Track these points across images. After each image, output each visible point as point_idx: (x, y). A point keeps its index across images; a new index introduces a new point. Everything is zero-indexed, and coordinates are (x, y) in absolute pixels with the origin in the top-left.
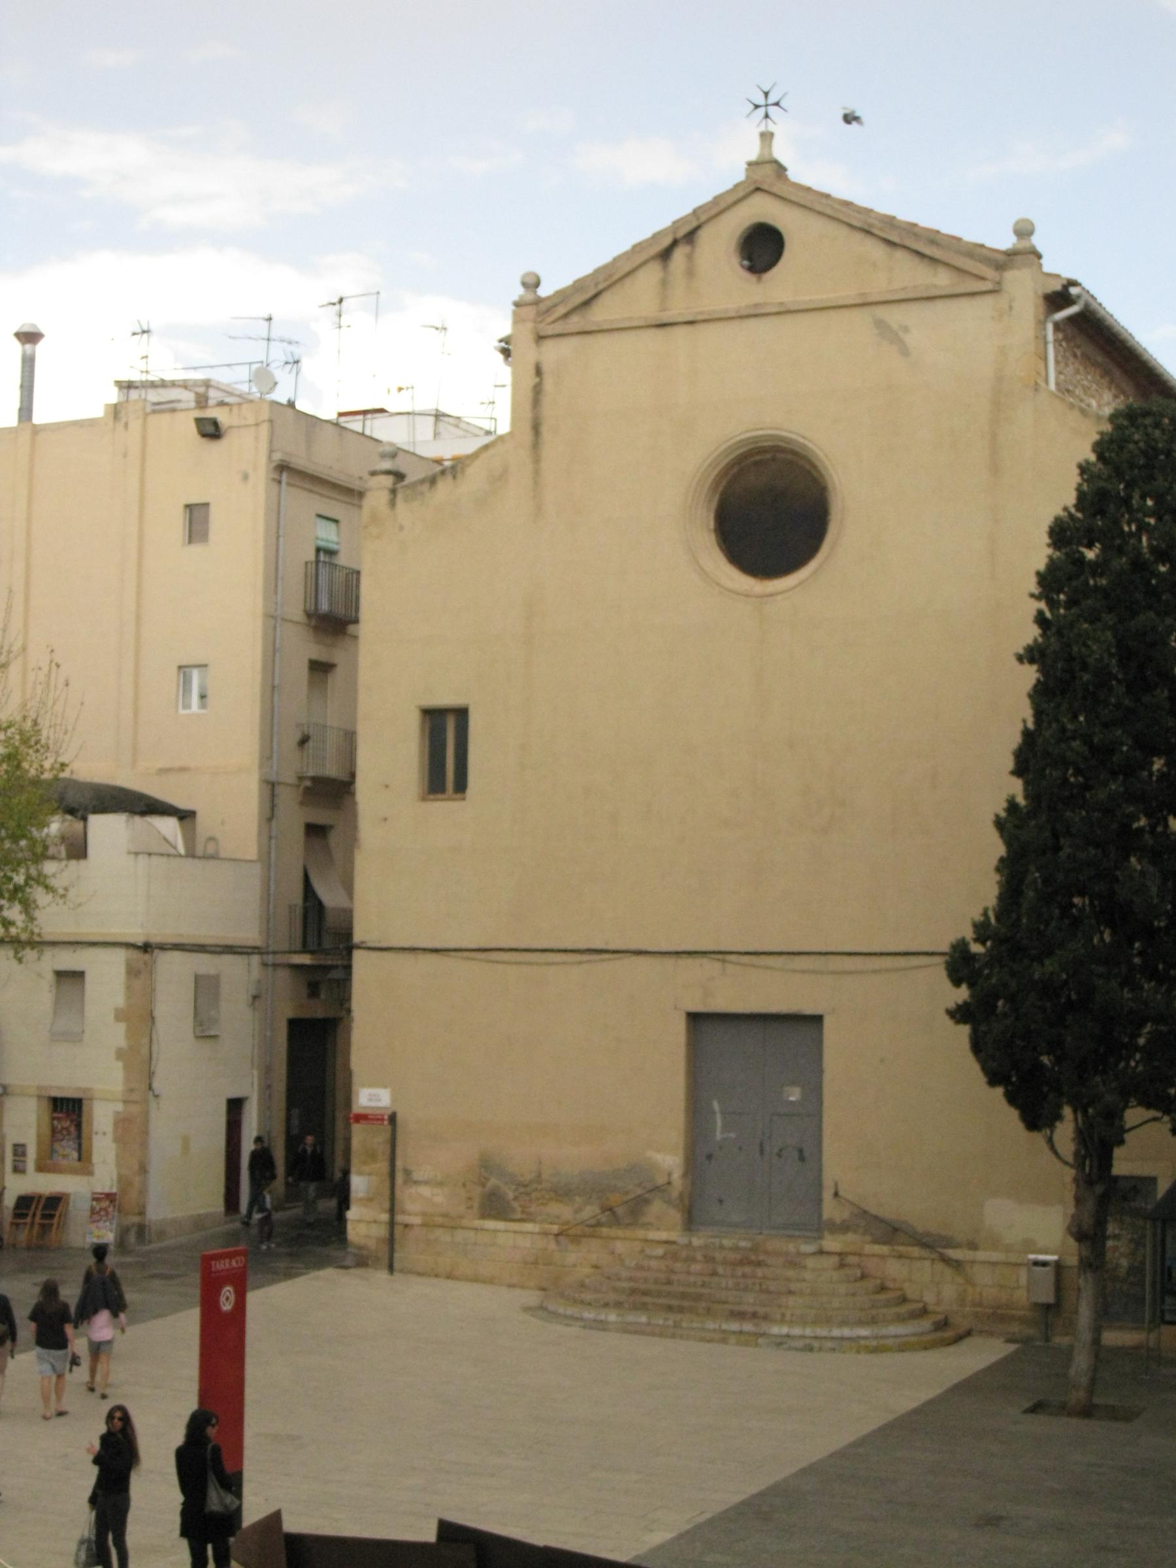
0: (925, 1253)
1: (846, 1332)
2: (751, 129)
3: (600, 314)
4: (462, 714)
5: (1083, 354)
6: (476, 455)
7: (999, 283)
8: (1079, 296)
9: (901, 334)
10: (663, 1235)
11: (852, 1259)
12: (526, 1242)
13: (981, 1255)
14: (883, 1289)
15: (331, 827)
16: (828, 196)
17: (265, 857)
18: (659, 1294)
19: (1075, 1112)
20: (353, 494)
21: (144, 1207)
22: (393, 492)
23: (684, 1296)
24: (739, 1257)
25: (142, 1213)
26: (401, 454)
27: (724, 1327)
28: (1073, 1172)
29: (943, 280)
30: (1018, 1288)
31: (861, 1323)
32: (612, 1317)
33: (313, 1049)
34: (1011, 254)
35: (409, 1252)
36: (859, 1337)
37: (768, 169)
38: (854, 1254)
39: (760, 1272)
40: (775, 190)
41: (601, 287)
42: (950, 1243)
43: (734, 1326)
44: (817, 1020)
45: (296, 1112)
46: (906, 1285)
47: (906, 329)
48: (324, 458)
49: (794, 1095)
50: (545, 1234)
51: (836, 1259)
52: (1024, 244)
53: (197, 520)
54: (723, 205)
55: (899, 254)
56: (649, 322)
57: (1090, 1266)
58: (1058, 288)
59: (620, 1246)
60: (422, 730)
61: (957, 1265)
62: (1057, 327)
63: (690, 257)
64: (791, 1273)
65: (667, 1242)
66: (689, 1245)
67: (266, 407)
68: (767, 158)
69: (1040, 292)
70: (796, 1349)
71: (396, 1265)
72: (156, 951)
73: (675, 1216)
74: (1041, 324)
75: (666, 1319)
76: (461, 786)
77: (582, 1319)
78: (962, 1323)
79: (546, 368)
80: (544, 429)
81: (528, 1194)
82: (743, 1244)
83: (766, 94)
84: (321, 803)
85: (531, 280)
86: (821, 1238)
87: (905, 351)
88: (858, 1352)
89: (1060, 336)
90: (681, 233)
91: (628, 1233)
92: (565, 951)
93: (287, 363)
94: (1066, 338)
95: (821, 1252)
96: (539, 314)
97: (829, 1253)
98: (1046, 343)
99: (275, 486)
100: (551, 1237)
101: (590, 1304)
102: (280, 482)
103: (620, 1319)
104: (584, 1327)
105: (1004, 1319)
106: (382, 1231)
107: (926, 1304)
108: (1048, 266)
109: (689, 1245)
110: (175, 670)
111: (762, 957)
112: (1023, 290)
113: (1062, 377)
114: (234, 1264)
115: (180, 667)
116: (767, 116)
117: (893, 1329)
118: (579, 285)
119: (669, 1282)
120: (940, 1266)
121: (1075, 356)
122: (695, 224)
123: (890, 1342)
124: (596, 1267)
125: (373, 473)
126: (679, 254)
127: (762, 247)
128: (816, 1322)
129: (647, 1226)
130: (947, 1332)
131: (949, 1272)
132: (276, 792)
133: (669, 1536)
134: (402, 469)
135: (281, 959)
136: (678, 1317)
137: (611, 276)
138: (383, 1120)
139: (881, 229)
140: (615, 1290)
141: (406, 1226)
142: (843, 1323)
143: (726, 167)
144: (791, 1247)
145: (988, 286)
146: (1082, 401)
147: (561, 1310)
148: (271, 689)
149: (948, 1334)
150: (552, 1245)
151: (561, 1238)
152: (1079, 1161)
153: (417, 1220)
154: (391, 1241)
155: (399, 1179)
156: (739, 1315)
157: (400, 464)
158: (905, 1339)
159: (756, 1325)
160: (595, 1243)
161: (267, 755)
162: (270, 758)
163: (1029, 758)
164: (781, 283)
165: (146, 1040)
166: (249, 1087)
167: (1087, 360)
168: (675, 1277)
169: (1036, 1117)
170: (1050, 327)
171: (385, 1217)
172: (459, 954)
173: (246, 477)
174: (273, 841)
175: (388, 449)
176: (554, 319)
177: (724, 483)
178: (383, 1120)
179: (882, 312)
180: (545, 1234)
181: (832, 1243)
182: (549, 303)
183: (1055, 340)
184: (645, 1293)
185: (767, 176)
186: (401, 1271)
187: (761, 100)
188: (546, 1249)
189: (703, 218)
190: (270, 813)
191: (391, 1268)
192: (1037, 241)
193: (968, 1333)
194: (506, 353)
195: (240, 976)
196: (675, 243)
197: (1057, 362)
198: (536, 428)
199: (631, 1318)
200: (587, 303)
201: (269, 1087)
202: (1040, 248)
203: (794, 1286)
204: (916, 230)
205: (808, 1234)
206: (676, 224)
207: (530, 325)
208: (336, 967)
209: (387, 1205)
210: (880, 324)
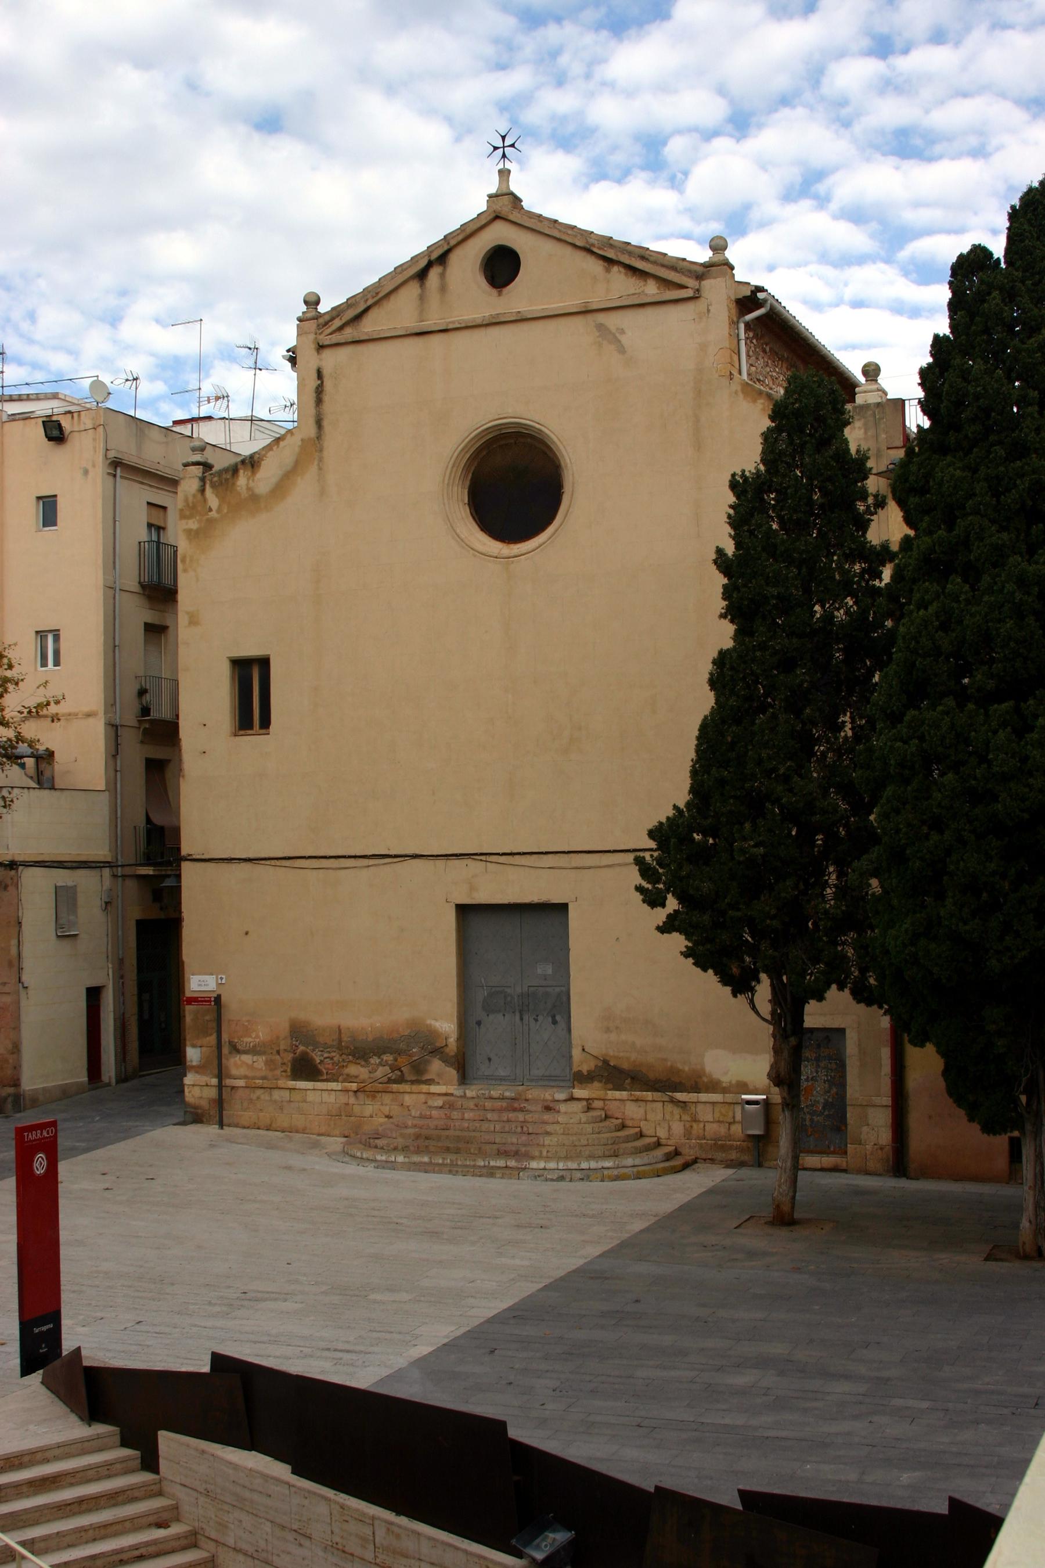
0: (657, 1095)
1: (593, 1164)
3: (369, 326)
4: (264, 663)
5: (771, 349)
6: (269, 448)
7: (698, 290)
8: (765, 301)
11: (597, 1104)
12: (331, 1098)
13: (704, 1097)
14: (623, 1126)
15: (169, 761)
16: (574, 227)
17: (112, 787)
19: (770, 977)
20: (171, 483)
21: (18, 1079)
22: (203, 480)
23: (458, 1139)
25: (16, 1083)
26: (209, 448)
27: (492, 1163)
28: (771, 1028)
29: (651, 290)
30: (734, 1122)
31: (605, 1157)
32: (400, 1159)
33: (156, 941)
34: (708, 265)
35: (234, 1110)
37: (505, 203)
39: (521, 1116)
40: (511, 217)
41: (370, 303)
43: (501, 1163)
44: (563, 908)
45: (146, 996)
46: (642, 1124)
48: (153, 456)
50: (346, 1091)
51: (585, 1103)
52: (718, 258)
53: (49, 509)
54: (468, 231)
56: (414, 331)
57: (788, 1105)
59: (408, 1099)
60: (233, 678)
61: (684, 1104)
62: (748, 326)
63: (442, 276)
64: (547, 1117)
65: (446, 1094)
66: (464, 1096)
67: (102, 412)
68: (505, 191)
69: (733, 298)
70: (552, 1180)
71: (225, 1120)
72: (21, 868)
73: (452, 1073)
74: (734, 324)
75: (444, 1159)
76: (266, 722)
77: (376, 1161)
79: (326, 372)
80: (325, 423)
82: (507, 1094)
83: (503, 138)
84: (150, 737)
85: (313, 299)
87: (622, 350)
88: (602, 1181)
89: (751, 335)
90: (434, 256)
92: (355, 857)
93: (127, 380)
94: (756, 336)
95: (572, 1098)
98: (739, 340)
99: (111, 478)
100: (351, 1094)
101: (382, 1148)
102: (115, 476)
103: (407, 1160)
105: (723, 1148)
106: (213, 1093)
107: (659, 1139)
110: (33, 634)
111: (517, 857)
112: (717, 294)
113: (753, 369)
114: (45, 1134)
115: (37, 632)
116: (504, 156)
117: (629, 1161)
118: (350, 303)
120: (669, 1107)
121: (764, 351)
122: (446, 248)
124: (388, 1117)
125: (186, 465)
126: (434, 274)
127: (501, 267)
128: (567, 1158)
129: (430, 1082)
130: (678, 1161)
131: (677, 1111)
133: (431, 1349)
134: (210, 461)
135: (128, 871)
136: (454, 1157)
137: (377, 294)
138: (210, 1001)
139: (599, 248)
140: (403, 1136)
141: (233, 1088)
142: (591, 1157)
143: (473, 204)
145: (689, 293)
146: (771, 389)
147: (359, 1154)
148: (113, 648)
149: (678, 1162)
150: (352, 1100)
151: (359, 1094)
152: (775, 1019)
153: (241, 1083)
154: (220, 1102)
155: (225, 1050)
157: (209, 456)
158: (641, 1168)
159: (516, 1161)
160: (387, 1098)
161: (111, 704)
162: (114, 704)
164: (520, 296)
165: (14, 942)
166: (104, 977)
167: (774, 354)
169: (741, 985)
170: (742, 326)
171: (214, 1081)
172: (268, 862)
173: (86, 472)
174: (119, 774)
175: (197, 444)
176: (333, 331)
177: (476, 464)
178: (210, 1001)
179: (601, 318)
180: (346, 1091)
182: (327, 318)
183: (747, 338)
184: (427, 1138)
185: (505, 206)
186: (229, 1126)
187: (500, 144)
188: (347, 1104)
189: (453, 242)
190: (115, 751)
191: (221, 1125)
194: (293, 361)
195: (91, 887)
196: (430, 265)
197: (748, 355)
199: (416, 1158)
200: (358, 317)
201: (122, 977)
202: (732, 261)
203: (549, 1128)
204: (611, 242)
207: (312, 337)
208: (169, 876)
209: (216, 1072)
210: (600, 327)
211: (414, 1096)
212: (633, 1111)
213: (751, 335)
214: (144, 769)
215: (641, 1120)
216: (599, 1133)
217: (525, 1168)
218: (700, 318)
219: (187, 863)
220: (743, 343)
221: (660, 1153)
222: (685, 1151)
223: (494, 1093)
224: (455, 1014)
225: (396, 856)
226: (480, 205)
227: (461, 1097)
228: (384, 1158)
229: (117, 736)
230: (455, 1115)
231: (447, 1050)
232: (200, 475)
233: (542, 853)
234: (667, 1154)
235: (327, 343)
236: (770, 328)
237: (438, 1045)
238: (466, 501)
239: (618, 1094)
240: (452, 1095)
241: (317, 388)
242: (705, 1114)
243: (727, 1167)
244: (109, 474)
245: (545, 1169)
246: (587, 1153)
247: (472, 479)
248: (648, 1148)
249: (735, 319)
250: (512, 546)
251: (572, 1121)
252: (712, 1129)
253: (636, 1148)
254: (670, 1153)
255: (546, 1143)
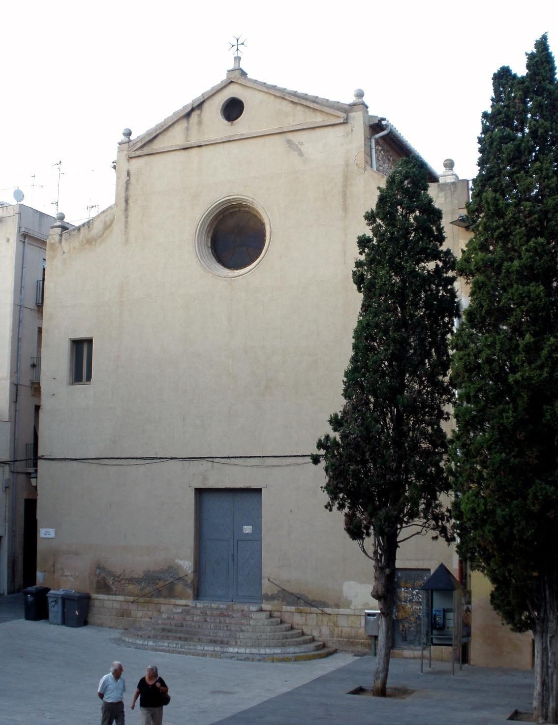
1: (268, 651)
2: (232, 53)
3: (157, 146)
4: (90, 341)
7: (347, 119)
9: (299, 146)
10: (183, 602)
12: (117, 605)
13: (341, 611)
14: (292, 628)
18: (176, 631)
22: (61, 235)
24: (219, 613)
29: (319, 119)
30: (360, 628)
31: (276, 646)
32: (151, 643)
34: (352, 106)
36: (274, 654)
37: (237, 73)
38: (278, 611)
39: (228, 620)
42: (325, 605)
43: (211, 648)
44: (259, 491)
47: (302, 144)
49: (248, 529)
51: (268, 613)
55: (299, 108)
58: (377, 122)
62: (377, 143)
63: (199, 116)
65: (185, 606)
66: (195, 607)
74: (368, 139)
75: (177, 644)
76: (89, 378)
78: (332, 646)
79: (132, 173)
80: (130, 201)
81: (120, 582)
82: (222, 606)
86: (262, 603)
87: (301, 154)
88: (273, 662)
91: (167, 601)
92: (137, 458)
94: (383, 150)
95: (261, 610)
96: (129, 147)
97: (265, 611)
98: (371, 149)
101: (141, 636)
102: (24, 242)
104: (136, 648)
105: (352, 644)
108: (372, 112)
109: (195, 607)
117: (291, 649)
119: (182, 626)
121: (389, 160)
123: (290, 656)
128: (253, 646)
129: (175, 597)
132: (19, 388)
140: (154, 629)
142: (268, 646)
144: (246, 608)
145: (342, 121)
156: (214, 642)
163: (355, 347)
164: (242, 126)
168: (185, 623)
170: (373, 141)
172: (87, 461)
173: (8, 240)
174: (17, 412)
179: (290, 136)
181: (266, 606)
182: (134, 142)
184: (169, 631)
185: (238, 76)
189: (206, 97)
192: (365, 99)
193: (335, 651)
194: (115, 167)
196: (193, 110)
197: (377, 159)
198: (127, 201)
200: (151, 141)
202: (367, 103)
205: (256, 601)
206: (194, 101)
210: (289, 142)
211: (167, 606)
212: (298, 619)
213: (380, 148)
214: (34, 411)
215: (303, 625)
216: (275, 632)
217: (226, 652)
218: (348, 135)
219: (42, 461)
220: (374, 151)
221: (312, 646)
222: (330, 644)
223: (214, 606)
224: (193, 556)
225: (161, 458)
226: (222, 77)
227: (194, 607)
228: (141, 642)
229: (17, 390)
230: (188, 618)
231: (187, 578)
232: (60, 233)
233: (247, 457)
234: (317, 646)
235: (133, 156)
236: (387, 142)
237: (181, 575)
238: (210, 245)
239: (289, 608)
240: (188, 606)
241: (127, 181)
242: (343, 622)
243: (355, 655)
244: (21, 241)
245: (237, 653)
246: (265, 644)
247: (213, 232)
248: (305, 642)
249: (369, 137)
250: (235, 271)
251: (258, 624)
252: (346, 630)
253: (297, 641)
254: (320, 645)
255: (241, 637)
